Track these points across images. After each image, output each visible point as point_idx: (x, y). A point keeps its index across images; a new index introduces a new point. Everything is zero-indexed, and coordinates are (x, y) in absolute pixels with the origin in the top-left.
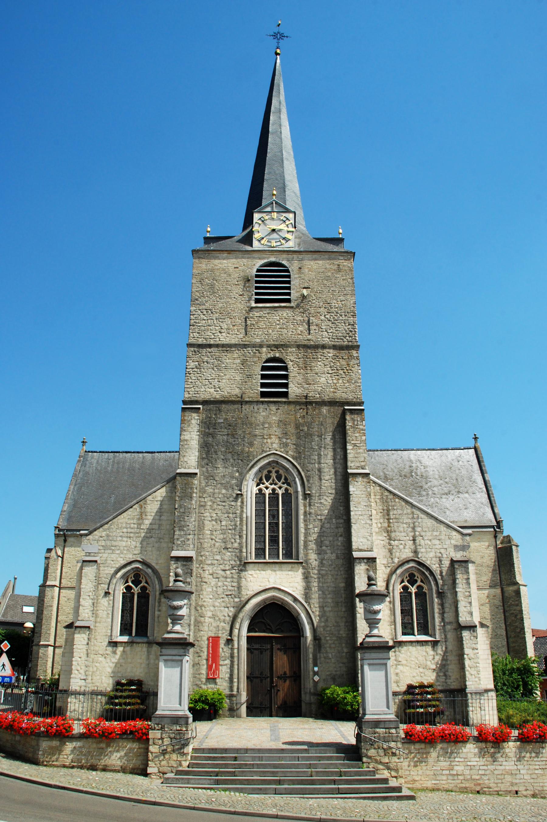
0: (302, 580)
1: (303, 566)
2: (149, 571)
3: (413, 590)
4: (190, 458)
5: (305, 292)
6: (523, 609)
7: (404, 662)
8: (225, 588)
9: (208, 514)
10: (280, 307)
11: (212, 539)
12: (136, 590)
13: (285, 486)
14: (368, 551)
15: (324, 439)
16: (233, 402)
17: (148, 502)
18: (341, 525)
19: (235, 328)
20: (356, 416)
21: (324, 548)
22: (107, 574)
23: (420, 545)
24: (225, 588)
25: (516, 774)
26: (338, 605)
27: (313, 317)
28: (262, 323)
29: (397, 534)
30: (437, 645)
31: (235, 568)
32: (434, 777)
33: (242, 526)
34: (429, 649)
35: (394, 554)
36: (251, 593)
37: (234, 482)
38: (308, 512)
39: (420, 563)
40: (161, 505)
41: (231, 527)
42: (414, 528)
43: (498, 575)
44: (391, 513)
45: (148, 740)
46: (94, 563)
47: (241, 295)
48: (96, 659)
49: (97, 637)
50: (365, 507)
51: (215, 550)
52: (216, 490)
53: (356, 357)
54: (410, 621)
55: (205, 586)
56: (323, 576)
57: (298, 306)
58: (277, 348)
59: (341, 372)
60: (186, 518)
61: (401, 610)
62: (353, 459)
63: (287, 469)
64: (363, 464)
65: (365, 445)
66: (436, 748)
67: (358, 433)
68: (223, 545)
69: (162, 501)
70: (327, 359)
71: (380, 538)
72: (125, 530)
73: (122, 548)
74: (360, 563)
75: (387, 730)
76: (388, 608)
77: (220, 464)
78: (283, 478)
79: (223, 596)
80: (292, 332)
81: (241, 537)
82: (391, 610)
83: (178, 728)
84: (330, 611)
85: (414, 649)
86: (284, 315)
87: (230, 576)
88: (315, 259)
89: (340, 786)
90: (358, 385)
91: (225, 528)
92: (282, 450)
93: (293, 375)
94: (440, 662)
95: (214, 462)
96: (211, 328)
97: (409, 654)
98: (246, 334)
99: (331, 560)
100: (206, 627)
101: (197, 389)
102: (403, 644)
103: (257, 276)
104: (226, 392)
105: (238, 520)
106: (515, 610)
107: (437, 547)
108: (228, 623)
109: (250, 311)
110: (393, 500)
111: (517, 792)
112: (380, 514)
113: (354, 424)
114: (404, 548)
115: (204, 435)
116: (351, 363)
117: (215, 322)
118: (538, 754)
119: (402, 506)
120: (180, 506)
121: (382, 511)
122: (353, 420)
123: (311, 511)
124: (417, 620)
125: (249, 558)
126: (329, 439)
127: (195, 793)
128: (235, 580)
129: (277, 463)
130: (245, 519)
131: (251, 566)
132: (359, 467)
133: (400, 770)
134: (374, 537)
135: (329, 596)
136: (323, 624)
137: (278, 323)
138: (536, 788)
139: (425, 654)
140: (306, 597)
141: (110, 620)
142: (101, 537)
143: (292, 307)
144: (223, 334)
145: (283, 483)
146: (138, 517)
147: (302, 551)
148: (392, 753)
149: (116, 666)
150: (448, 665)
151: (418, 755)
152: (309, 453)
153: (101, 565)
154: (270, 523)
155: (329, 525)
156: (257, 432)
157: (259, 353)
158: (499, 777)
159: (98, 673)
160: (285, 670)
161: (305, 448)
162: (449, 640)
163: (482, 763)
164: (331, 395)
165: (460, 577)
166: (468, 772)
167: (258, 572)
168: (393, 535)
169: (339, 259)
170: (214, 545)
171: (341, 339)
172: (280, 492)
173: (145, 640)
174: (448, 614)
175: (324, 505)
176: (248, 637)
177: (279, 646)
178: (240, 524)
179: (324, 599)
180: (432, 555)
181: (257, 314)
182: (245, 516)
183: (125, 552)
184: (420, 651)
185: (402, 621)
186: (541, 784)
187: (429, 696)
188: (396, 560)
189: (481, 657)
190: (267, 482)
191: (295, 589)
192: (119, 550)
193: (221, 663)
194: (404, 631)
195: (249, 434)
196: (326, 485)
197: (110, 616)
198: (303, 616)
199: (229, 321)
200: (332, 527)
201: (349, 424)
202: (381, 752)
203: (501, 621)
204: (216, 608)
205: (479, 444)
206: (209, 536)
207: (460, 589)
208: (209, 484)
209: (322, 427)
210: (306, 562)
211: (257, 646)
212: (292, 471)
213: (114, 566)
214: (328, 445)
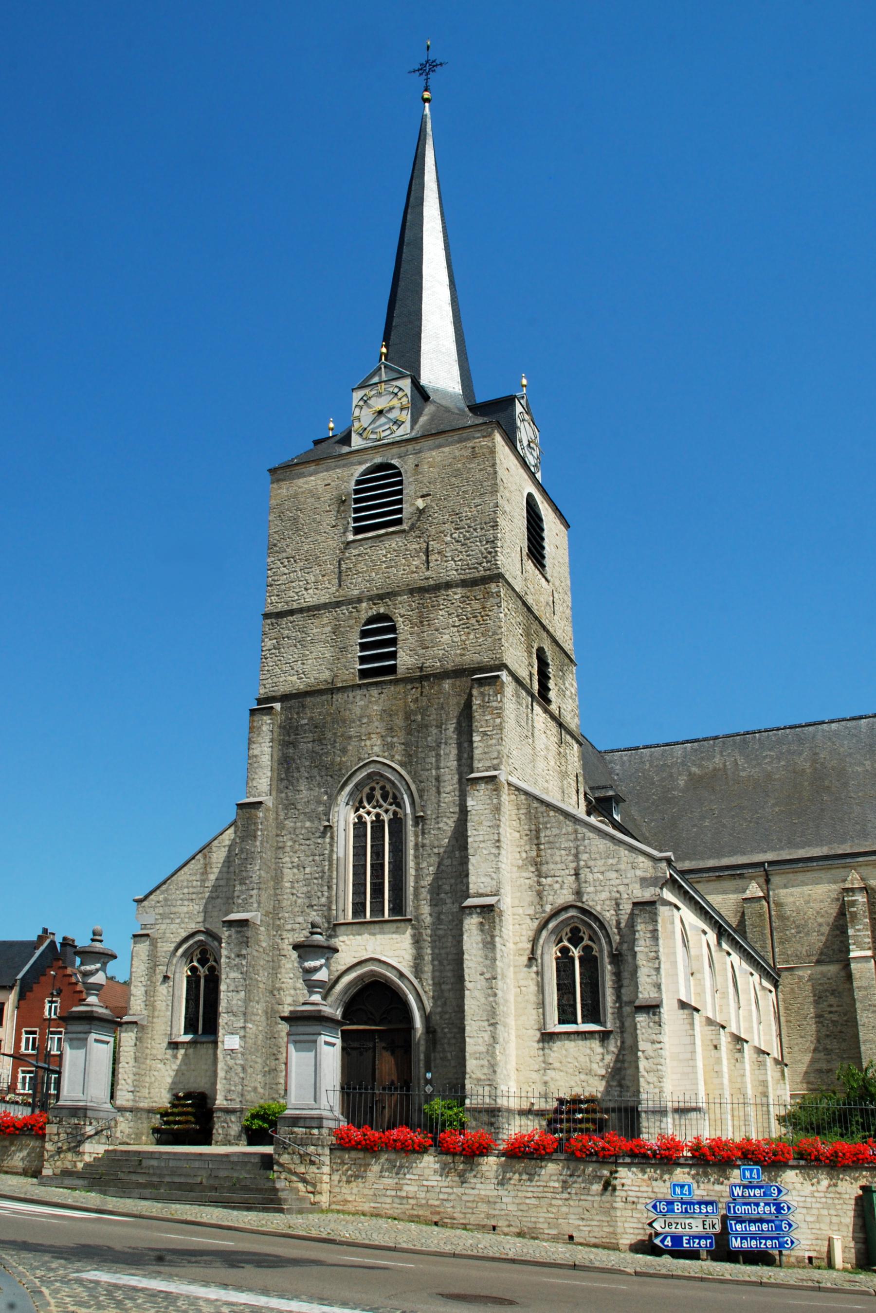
0: (410, 946)
1: (412, 925)
3: (576, 953)
4: (260, 781)
7: (557, 1065)
9: (287, 859)
10: (387, 534)
11: (293, 894)
12: (202, 971)
13: (393, 807)
14: (491, 895)
15: (445, 730)
16: (320, 692)
17: (214, 849)
19: (325, 578)
20: (487, 688)
21: (442, 896)
23: (586, 882)
25: (495, 1203)
27: (434, 540)
28: (362, 565)
29: (551, 866)
30: (608, 1038)
32: (373, 1198)
33: (332, 872)
34: (596, 1044)
35: (545, 899)
37: (321, 808)
38: (420, 844)
39: (584, 911)
40: (229, 851)
41: (317, 875)
42: (576, 856)
44: (542, 835)
45: (44, 1135)
46: (145, 938)
47: (334, 526)
48: (154, 1066)
49: (155, 1037)
50: (488, 829)
51: (296, 909)
53: (496, 592)
55: (284, 961)
56: (440, 938)
57: (412, 528)
58: (382, 600)
60: (249, 866)
61: (558, 985)
62: (481, 756)
64: (495, 762)
65: (499, 732)
66: (379, 1159)
67: (490, 714)
68: (306, 901)
69: (230, 846)
70: (453, 604)
71: (525, 875)
72: (186, 891)
73: (182, 915)
74: (471, 914)
75: (308, 1130)
76: (534, 982)
77: (303, 786)
78: (391, 795)
80: (404, 570)
81: (329, 888)
82: (538, 985)
84: (449, 990)
85: (572, 1044)
86: (393, 545)
88: (440, 446)
90: (497, 637)
91: (309, 876)
92: (386, 754)
94: (612, 1065)
95: (295, 784)
96: (293, 584)
97: (564, 1052)
98: (340, 586)
99: (452, 914)
101: (275, 680)
102: (555, 1037)
103: (357, 492)
104: (312, 679)
105: (327, 863)
107: (612, 882)
109: (345, 549)
111: (494, 1228)
112: (525, 838)
113: (483, 701)
114: (561, 888)
115: (283, 746)
118: (531, 1177)
119: (560, 823)
120: (241, 851)
121: (528, 833)
122: (482, 694)
123: (425, 841)
126: (452, 729)
129: (382, 776)
130: (335, 862)
131: (343, 928)
132: (489, 767)
133: (319, 1184)
135: (448, 968)
136: (439, 1009)
137: (384, 559)
138: (525, 1224)
139: (588, 1051)
140: (416, 970)
141: (169, 1013)
142: (158, 902)
143: (404, 531)
144: (309, 591)
145: (391, 804)
148: (310, 1160)
149: (176, 1075)
150: (625, 1069)
151: (353, 1167)
152: (423, 755)
154: (372, 865)
155: (450, 860)
156: (352, 732)
157: (357, 611)
158: (469, 1204)
159: (156, 1084)
161: (417, 747)
162: (628, 1030)
163: (446, 1184)
164: (458, 659)
166: (423, 1195)
167: (351, 937)
168: (544, 868)
169: (474, 438)
170: (296, 902)
171: (474, 568)
175: (444, 831)
177: (384, 1045)
178: (329, 869)
179: (441, 971)
180: (604, 895)
181: (355, 552)
182: (335, 857)
183: (186, 920)
184: (581, 1048)
186: (533, 1219)
187: (580, 1116)
188: (548, 908)
190: (369, 804)
191: (401, 959)
195: (342, 735)
196: (446, 800)
197: (170, 1008)
198: (411, 999)
199: (316, 569)
200: (455, 863)
201: (476, 702)
202: (296, 1158)
207: (642, 948)
208: (290, 815)
209: (443, 712)
210: (417, 918)
211: (356, 1045)
212: (399, 785)
213: (174, 940)
214: (451, 738)
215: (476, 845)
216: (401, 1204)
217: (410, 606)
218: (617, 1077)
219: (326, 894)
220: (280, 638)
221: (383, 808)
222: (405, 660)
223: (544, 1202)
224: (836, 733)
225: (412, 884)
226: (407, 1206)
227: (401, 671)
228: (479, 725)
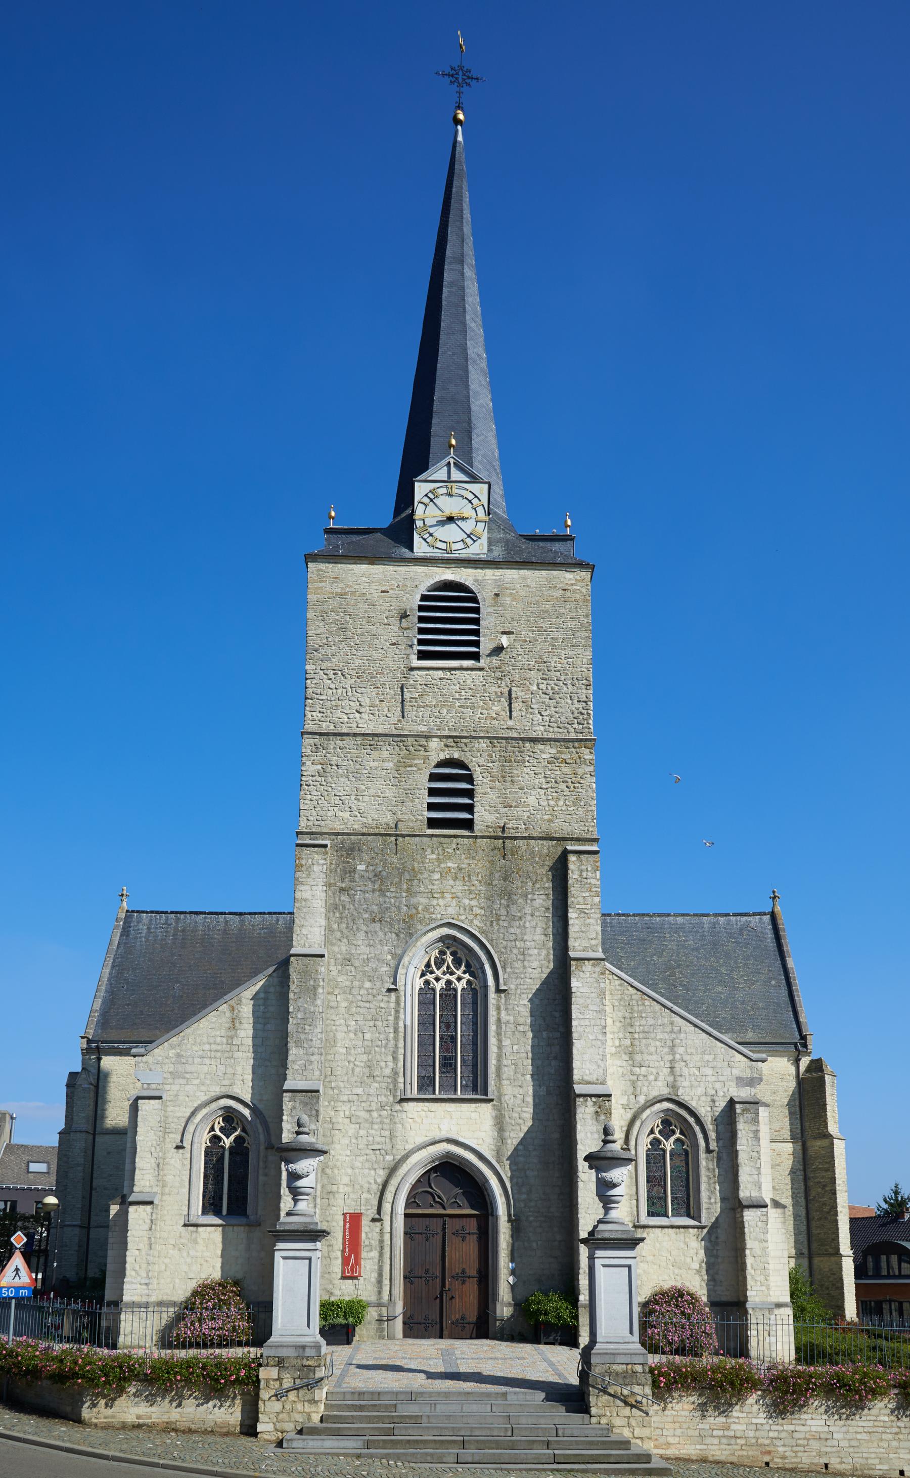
4: (312, 930)
5: (505, 641)
6: (836, 1176)
9: (342, 1022)
13: (467, 976)
15: (532, 900)
18: (556, 1041)
19: (384, 704)
22: (178, 1118)
25: (827, 1439)
31: (386, 1108)
32: (699, 1439)
35: (639, 1089)
36: (409, 1147)
42: (673, 1047)
43: (798, 1121)
47: (393, 644)
52: (354, 982)
54: (662, 1195)
61: (648, 1177)
62: (577, 935)
63: (470, 950)
71: (618, 1063)
79: (368, 1152)
80: (482, 714)
81: (395, 1059)
87: (378, 1120)
89: (556, 1452)
93: (483, 791)
100: (339, 1200)
105: (392, 1030)
106: (823, 1177)
108: (375, 1194)
113: (581, 876)
114: (656, 1080)
116: (580, 771)
117: (350, 694)
121: (623, 1020)
124: (672, 1194)
125: (409, 1091)
127: (335, 1462)
130: (401, 1030)
134: (609, 1062)
136: (524, 1197)
137: (457, 696)
139: (682, 1245)
140: (498, 1153)
145: (464, 972)
147: (493, 1082)
152: (505, 924)
153: (168, 1103)
154: (441, 1038)
160: (464, 1266)
165: (743, 1128)
170: (353, 1070)
172: (460, 986)
173: (243, 1220)
176: (405, 1214)
180: (700, 1091)
182: (401, 1024)
185: (648, 1195)
186: (865, 1455)
188: (642, 1100)
189: (772, 1254)
191: (481, 1142)
194: (653, 1209)
196: (533, 976)
199: (371, 692)
203: (799, 1193)
204: (357, 1171)
205: (778, 909)
206: (343, 1057)
215: (581, 1029)
217: (491, 756)
222: (483, 817)
223: (875, 1437)
224: (682, 928)
226: (736, 1447)
227: (479, 827)
228: (576, 901)
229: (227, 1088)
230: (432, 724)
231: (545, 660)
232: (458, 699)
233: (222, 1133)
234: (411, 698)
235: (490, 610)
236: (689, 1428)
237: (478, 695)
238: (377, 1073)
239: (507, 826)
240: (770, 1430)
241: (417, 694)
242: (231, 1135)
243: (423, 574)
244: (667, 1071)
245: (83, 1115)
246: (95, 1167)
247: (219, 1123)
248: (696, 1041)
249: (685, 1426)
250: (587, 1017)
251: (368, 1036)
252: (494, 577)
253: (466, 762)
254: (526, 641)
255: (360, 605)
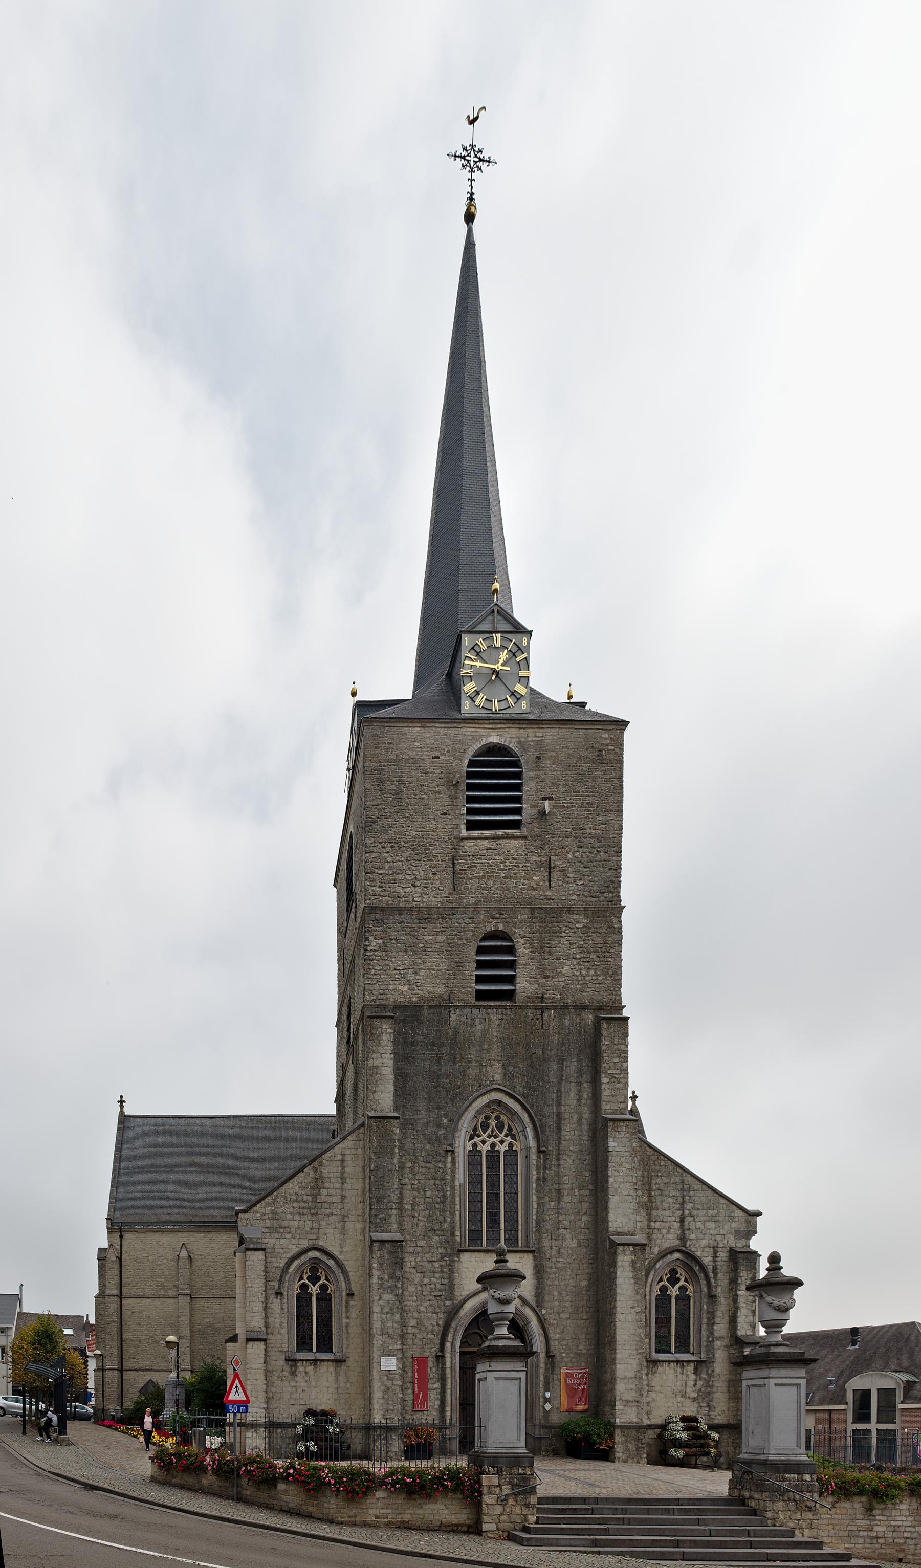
2: (331, 1263)
8: (433, 1286)
9: (407, 1180)
13: (509, 1139)
23: (689, 1229)
24: (433, 1286)
26: (578, 1310)
29: (661, 1212)
31: (446, 1258)
44: (654, 1182)
47: (445, 814)
51: (418, 1233)
59: (593, 956)
72: (296, 1205)
73: (293, 1230)
79: (431, 1298)
83: (521, 1471)
84: (567, 1319)
92: (508, 1083)
97: (665, 1377)
101: (382, 987)
107: (711, 1232)
108: (438, 1334)
110: (656, 1163)
114: (668, 1232)
128: (446, 1276)
135: (567, 1298)
145: (506, 1136)
146: (312, 1184)
150: (713, 1393)
166: (890, 1534)
168: (654, 1213)
174: (719, 1326)
176: (460, 1352)
180: (704, 1242)
192: (290, 1233)
193: (430, 1386)
200: (574, 1200)
215: (616, 1186)
216: (871, 1544)
218: (706, 1399)
219: (448, 1219)
220: (387, 939)
221: (499, 1139)
222: (524, 986)
225: (534, 1217)
227: (520, 997)
229: (314, 1241)
230: (480, 896)
231: (581, 826)
232: (503, 870)
233: (309, 1281)
234: (461, 870)
235: (532, 774)
236: (840, 1530)
237: (521, 866)
238: (438, 1227)
239: (545, 996)
240: (905, 1531)
241: (466, 866)
242: (317, 1283)
243: (470, 737)
244: (677, 1225)
245: (113, 1282)
246: (123, 1323)
247: (307, 1273)
248: (702, 1198)
249: (837, 1528)
250: (621, 1174)
251: (429, 1194)
252: (536, 739)
253: (510, 933)
254: (564, 807)
255: (413, 773)
